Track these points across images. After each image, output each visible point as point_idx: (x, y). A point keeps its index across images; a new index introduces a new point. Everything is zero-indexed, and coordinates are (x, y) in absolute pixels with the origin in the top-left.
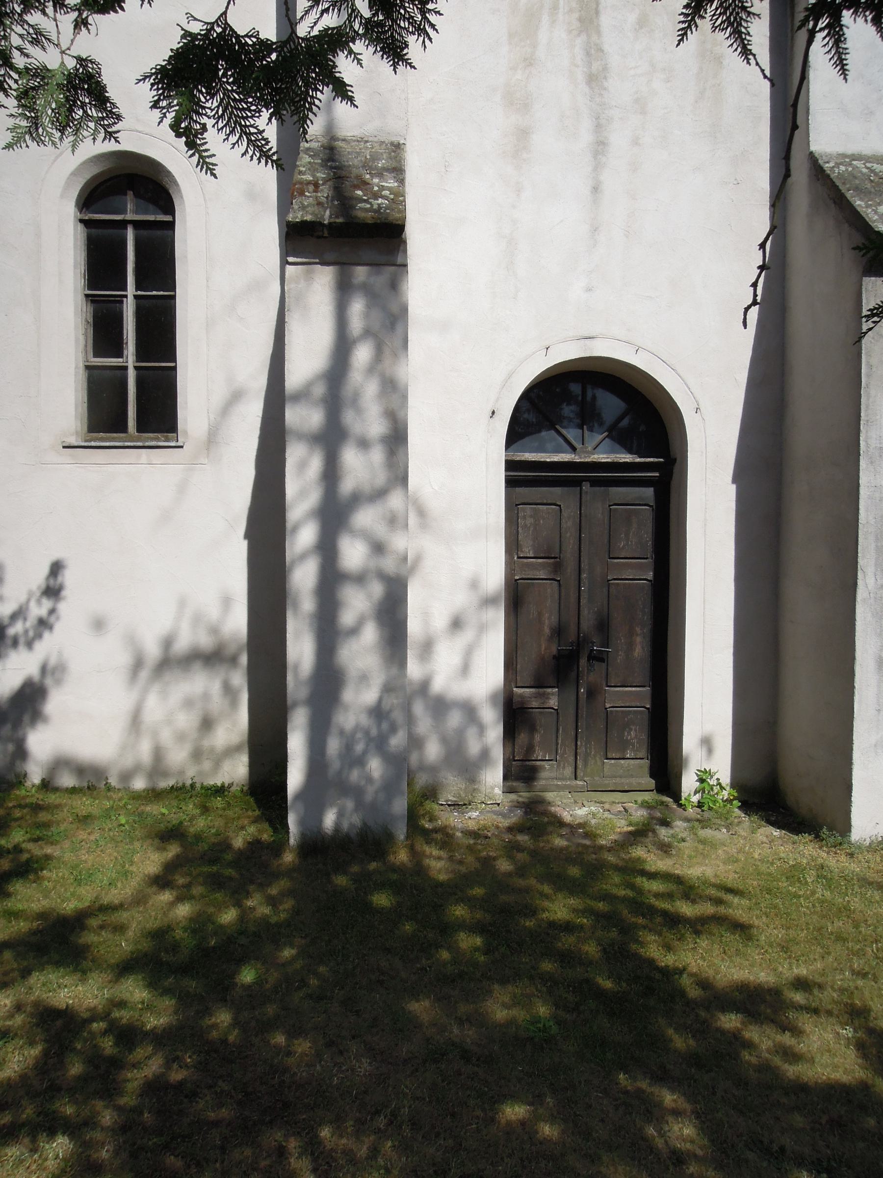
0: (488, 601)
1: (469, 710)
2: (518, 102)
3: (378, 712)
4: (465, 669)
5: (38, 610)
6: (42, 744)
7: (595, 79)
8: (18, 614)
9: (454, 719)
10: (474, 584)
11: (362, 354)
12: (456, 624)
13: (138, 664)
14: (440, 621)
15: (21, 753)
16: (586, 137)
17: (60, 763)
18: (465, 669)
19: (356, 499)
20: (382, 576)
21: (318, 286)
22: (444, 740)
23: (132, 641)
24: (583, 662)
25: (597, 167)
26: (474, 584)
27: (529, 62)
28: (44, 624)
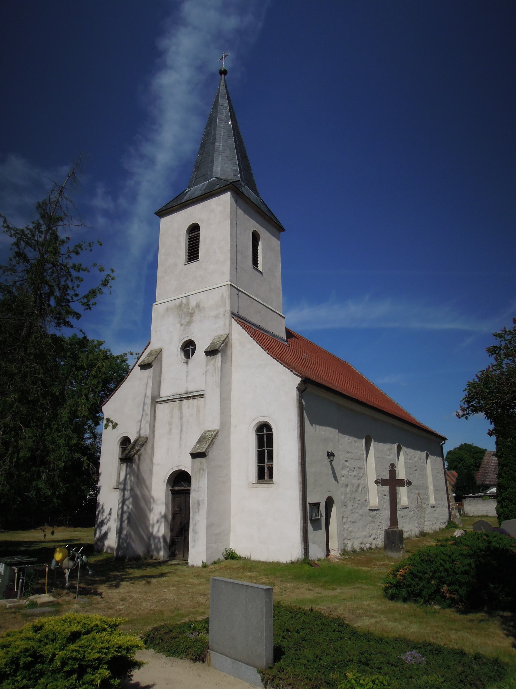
1: (159, 538)
2: (170, 424)
3: (126, 535)
4: (158, 531)
5: (108, 518)
6: (107, 543)
7: (181, 418)
8: (106, 518)
9: (157, 540)
10: (160, 513)
11: (128, 477)
12: (158, 521)
14: (155, 521)
15: (104, 545)
16: (180, 429)
17: (109, 547)
18: (158, 531)
19: (127, 499)
21: (124, 466)
25: (181, 434)
26: (160, 513)
27: (172, 417)
28: (109, 520)
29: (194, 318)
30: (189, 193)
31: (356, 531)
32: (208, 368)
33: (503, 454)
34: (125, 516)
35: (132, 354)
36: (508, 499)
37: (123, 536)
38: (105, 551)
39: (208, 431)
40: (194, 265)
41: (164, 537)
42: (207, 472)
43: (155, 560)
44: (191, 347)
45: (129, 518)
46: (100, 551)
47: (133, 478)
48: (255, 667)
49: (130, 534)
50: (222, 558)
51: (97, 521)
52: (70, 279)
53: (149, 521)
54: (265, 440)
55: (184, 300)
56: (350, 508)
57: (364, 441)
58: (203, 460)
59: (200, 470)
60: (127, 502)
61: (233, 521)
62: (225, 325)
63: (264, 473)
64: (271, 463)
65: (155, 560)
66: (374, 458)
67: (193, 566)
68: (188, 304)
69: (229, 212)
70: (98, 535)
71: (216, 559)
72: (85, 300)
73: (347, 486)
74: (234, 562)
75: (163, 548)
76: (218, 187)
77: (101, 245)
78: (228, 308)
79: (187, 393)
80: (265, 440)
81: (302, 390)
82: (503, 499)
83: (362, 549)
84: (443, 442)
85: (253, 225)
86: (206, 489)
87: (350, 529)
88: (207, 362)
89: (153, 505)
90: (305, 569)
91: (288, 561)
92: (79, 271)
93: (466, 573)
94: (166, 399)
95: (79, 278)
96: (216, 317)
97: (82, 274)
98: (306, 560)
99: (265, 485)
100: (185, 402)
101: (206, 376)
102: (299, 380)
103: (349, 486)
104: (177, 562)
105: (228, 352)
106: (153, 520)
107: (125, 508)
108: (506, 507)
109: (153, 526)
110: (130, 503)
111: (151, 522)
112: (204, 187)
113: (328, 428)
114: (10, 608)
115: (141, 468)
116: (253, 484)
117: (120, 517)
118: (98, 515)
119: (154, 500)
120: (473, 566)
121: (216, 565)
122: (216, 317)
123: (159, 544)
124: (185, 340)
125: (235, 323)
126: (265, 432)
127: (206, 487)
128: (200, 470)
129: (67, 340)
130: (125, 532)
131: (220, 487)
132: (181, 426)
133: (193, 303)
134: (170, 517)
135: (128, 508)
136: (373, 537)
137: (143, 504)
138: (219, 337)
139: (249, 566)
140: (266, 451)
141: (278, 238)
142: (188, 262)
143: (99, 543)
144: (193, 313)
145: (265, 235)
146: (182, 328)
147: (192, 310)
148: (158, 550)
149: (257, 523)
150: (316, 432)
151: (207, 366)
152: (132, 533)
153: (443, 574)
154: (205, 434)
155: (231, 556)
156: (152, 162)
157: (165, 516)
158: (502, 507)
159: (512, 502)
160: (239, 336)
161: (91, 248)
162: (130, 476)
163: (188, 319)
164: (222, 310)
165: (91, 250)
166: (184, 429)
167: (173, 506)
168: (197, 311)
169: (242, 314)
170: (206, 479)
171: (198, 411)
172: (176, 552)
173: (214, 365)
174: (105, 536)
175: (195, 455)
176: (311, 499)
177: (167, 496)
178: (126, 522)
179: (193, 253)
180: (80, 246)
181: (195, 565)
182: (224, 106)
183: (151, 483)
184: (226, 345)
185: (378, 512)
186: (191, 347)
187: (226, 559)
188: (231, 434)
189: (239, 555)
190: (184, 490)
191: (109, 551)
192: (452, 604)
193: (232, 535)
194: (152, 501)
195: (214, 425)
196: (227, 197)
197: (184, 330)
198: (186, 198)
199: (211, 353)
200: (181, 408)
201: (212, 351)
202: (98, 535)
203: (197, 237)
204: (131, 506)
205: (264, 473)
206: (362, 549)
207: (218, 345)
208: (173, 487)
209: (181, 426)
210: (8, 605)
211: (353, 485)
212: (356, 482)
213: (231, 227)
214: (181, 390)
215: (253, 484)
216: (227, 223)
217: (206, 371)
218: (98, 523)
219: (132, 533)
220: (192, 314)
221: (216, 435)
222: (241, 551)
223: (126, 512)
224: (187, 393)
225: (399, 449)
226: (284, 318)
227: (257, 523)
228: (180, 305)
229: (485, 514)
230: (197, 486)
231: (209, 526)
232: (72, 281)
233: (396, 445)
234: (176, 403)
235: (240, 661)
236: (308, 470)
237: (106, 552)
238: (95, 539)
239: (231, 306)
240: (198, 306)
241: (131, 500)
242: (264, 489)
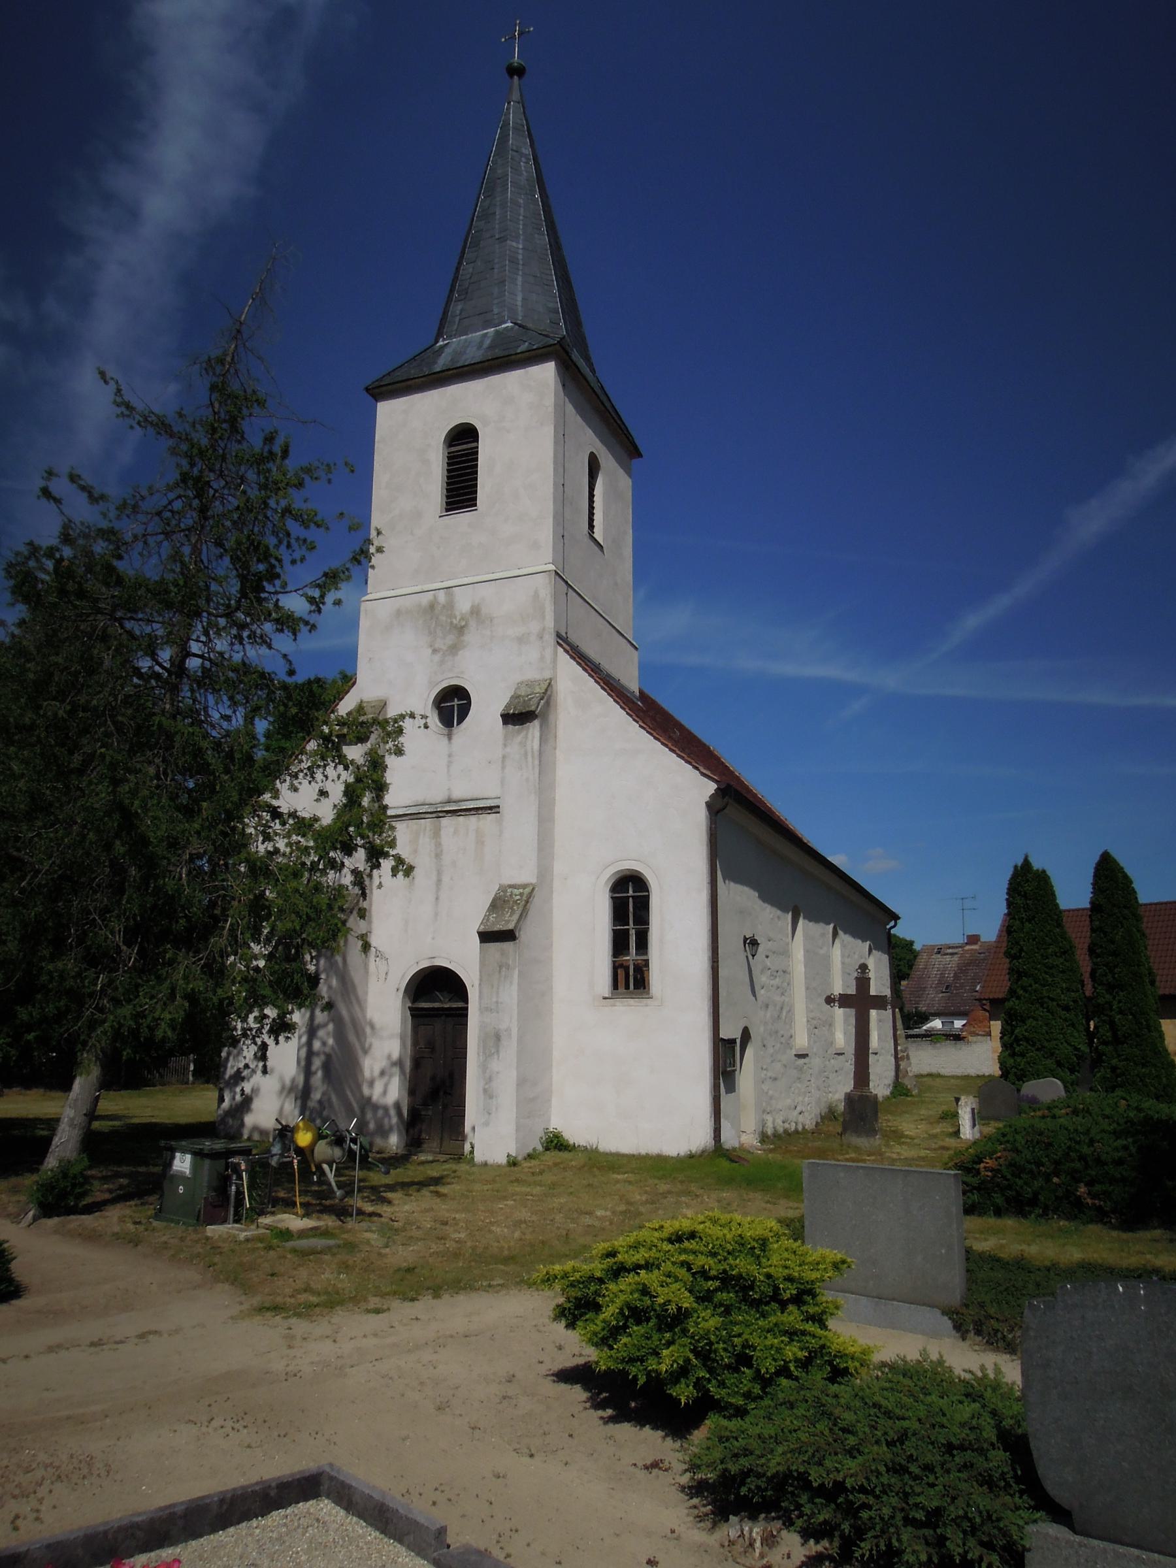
0: (394, 1064)
1: (386, 1109)
3: (320, 1102)
4: (385, 1093)
6: (249, 1120)
7: (438, 856)
9: (380, 1113)
10: (389, 1057)
12: (382, 1073)
13: (283, 1088)
14: (377, 1072)
15: (242, 1124)
16: (434, 878)
17: (255, 1128)
18: (385, 1093)
19: (319, 1027)
20: (325, 1053)
22: (376, 1123)
23: (282, 1079)
24: (441, 1093)
26: (389, 1057)
29: (467, 638)
30: (448, 351)
31: (787, 1095)
32: (508, 750)
33: (1021, 950)
34: (317, 1063)
35: (412, 716)
36: (1027, 1040)
37: (312, 1104)
38: (245, 1137)
39: (511, 886)
40: (462, 518)
41: (397, 1106)
42: (516, 972)
43: (378, 1153)
44: (456, 702)
45: (327, 1067)
46: (235, 1136)
47: (334, 982)
48: (937, 1307)
49: (329, 1099)
50: (540, 1148)
51: (224, 1073)
52: (285, 543)
53: (361, 1071)
54: (631, 909)
55: (442, 597)
56: (771, 1050)
57: (790, 916)
58: (507, 946)
59: (500, 967)
60: (321, 1033)
61: (558, 1074)
62: (542, 658)
63: (630, 977)
64: (644, 957)
65: (378, 1153)
66: (802, 952)
67: (486, 1164)
68: (450, 606)
69: (551, 409)
70: (226, 1104)
71: (530, 1150)
72: (316, 593)
73: (767, 1006)
74: (565, 1155)
75: (395, 1128)
76: (524, 347)
77: (352, 471)
78: (550, 623)
79: (449, 802)
80: (631, 909)
81: (715, 808)
82: (1017, 1040)
83: (786, 1131)
84: (892, 923)
85: (588, 440)
86: (515, 1007)
87: (771, 1092)
88: (506, 738)
89: (370, 1040)
90: (718, 1165)
91: (682, 1154)
92: (307, 527)
93: (1119, 1162)
94: (400, 812)
95: (305, 541)
96: (521, 640)
97: (312, 534)
98: (718, 1150)
99: (631, 1001)
100: (446, 821)
101: (503, 768)
102: (712, 787)
103: (771, 1008)
104: (430, 1158)
105: (551, 717)
106: (372, 1071)
107: (317, 1045)
108: (1022, 1055)
109: (371, 1084)
110: (328, 1034)
111: (367, 1074)
112: (487, 342)
113: (746, 889)
114: (247, 1240)
115: (349, 959)
116: (605, 998)
117: (303, 1063)
118: (227, 1059)
119: (372, 1027)
120: (1133, 1150)
121: (534, 1162)
122: (521, 640)
123: (386, 1121)
124: (445, 684)
125: (564, 658)
126: (631, 893)
127: (515, 1001)
128: (500, 967)
129: (330, 682)
130: (316, 1096)
131: (536, 1006)
132: (439, 873)
133: (463, 604)
134: (408, 1064)
135: (324, 1044)
136: (799, 1109)
137: (352, 1038)
138: (530, 684)
139: (602, 1164)
140: (632, 933)
141: (629, 472)
142: (447, 510)
143: (230, 1121)
144: (462, 627)
145: (607, 461)
146: (437, 657)
147: (462, 619)
148: (384, 1132)
149: (607, 1076)
150: (736, 895)
151: (505, 745)
152: (334, 1099)
153: (1078, 1165)
154: (505, 891)
155: (556, 1143)
156: (133, 214)
157: (399, 1063)
158: (1013, 1055)
159: (1033, 1045)
160: (571, 681)
161: (330, 476)
162: (328, 976)
163: (450, 639)
164: (535, 627)
165: (329, 481)
166: (446, 879)
167: (415, 1043)
168: (473, 623)
169: (574, 638)
170: (515, 987)
171: (480, 842)
172: (424, 1136)
173: (523, 744)
174: (246, 1103)
175: (487, 937)
176: (724, 1034)
177: (403, 1021)
178: (320, 1074)
179: (461, 490)
180: (308, 470)
181: (490, 1161)
182: (522, 155)
183: (366, 993)
184: (548, 703)
185: (806, 1060)
186: (456, 702)
187: (547, 1149)
188: (555, 895)
189: (571, 1142)
190: (443, 1009)
191: (256, 1137)
192: (1101, 1216)
193: (554, 1101)
194: (368, 1030)
195: (522, 873)
196: (546, 372)
197: (442, 662)
198: (442, 363)
199: (517, 717)
200: (437, 834)
201: (521, 714)
202: (226, 1104)
203: (473, 455)
204: (331, 1041)
205: (630, 977)
206: (786, 1131)
207: (535, 701)
208: (414, 1001)
209: (439, 873)
210: (242, 1236)
211: (775, 1005)
212: (778, 999)
213: (556, 443)
214: (436, 795)
215: (605, 998)
216: (549, 431)
217: (504, 757)
218: (227, 1076)
219: (334, 1099)
220: (461, 630)
221: (530, 894)
222: (576, 1134)
223: (318, 1054)
224: (449, 802)
225: (835, 934)
226: (636, 648)
227: (607, 1076)
228: (432, 606)
229: (934, 1071)
230: (494, 1000)
231: (521, 1082)
232: (289, 546)
233: (832, 926)
234: (426, 823)
235: (894, 1299)
236: (722, 973)
237: (249, 1139)
238: (220, 1112)
239: (556, 621)
240: (475, 611)
241: (331, 1027)
242: (628, 1010)
